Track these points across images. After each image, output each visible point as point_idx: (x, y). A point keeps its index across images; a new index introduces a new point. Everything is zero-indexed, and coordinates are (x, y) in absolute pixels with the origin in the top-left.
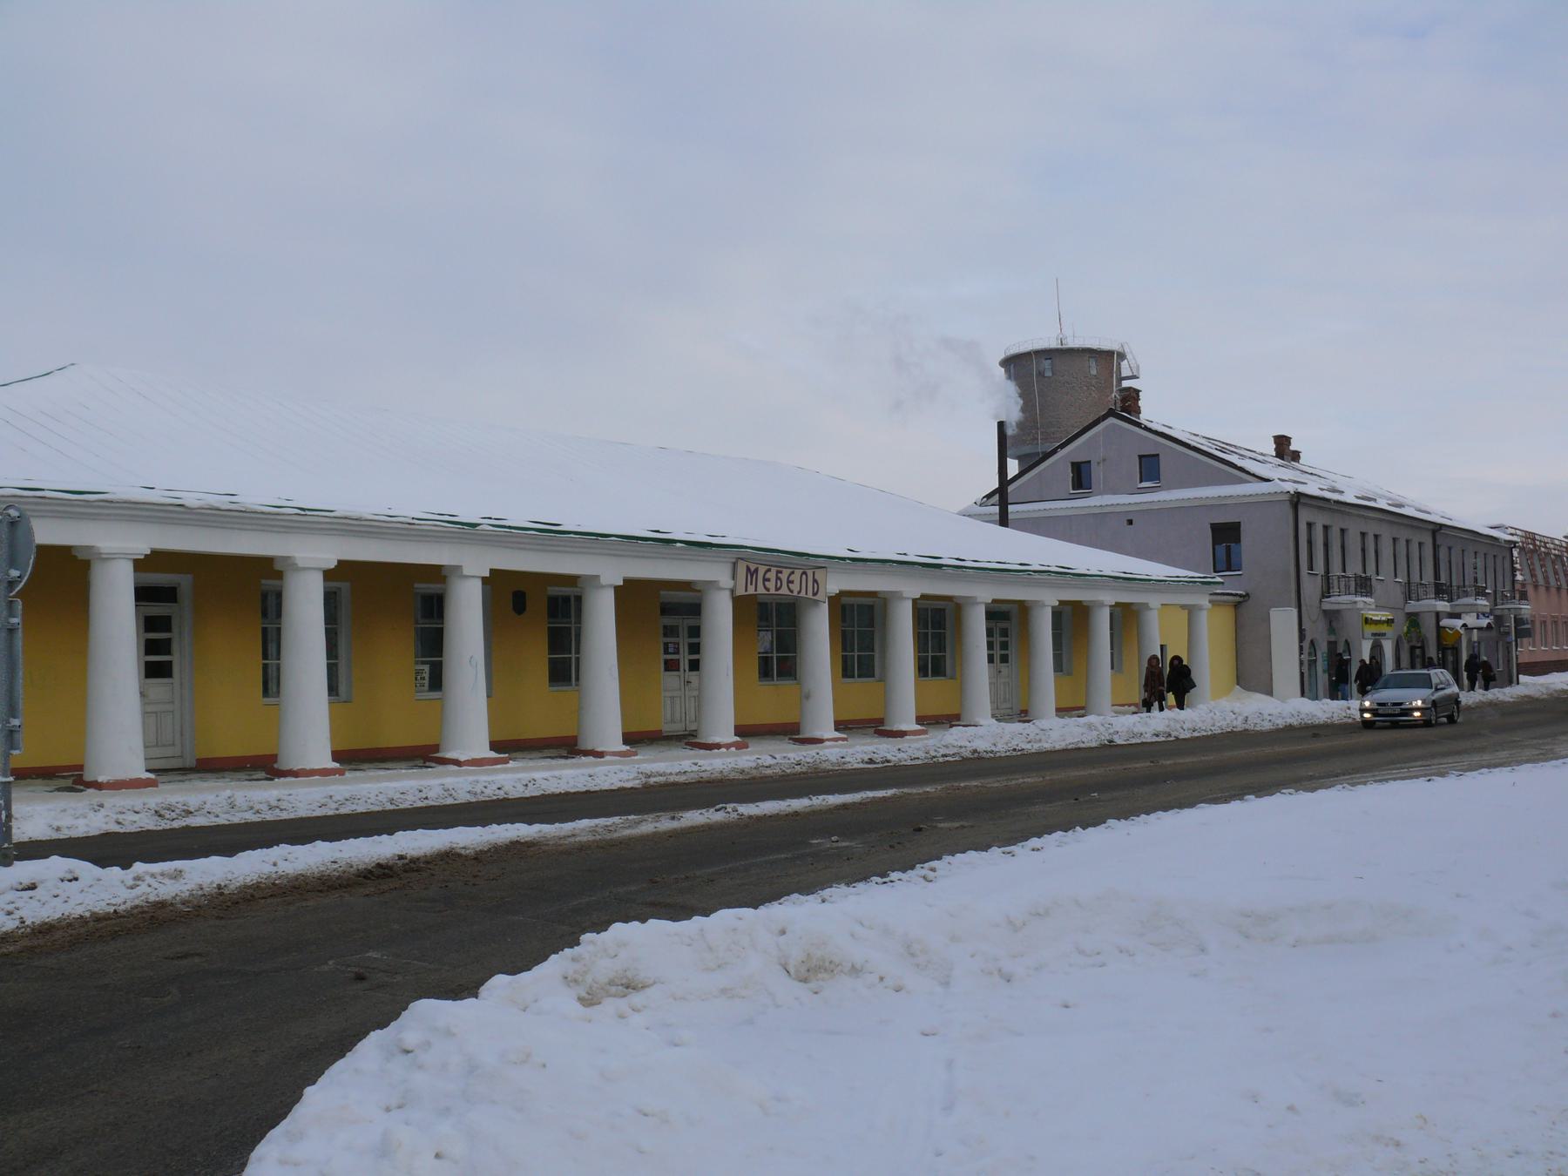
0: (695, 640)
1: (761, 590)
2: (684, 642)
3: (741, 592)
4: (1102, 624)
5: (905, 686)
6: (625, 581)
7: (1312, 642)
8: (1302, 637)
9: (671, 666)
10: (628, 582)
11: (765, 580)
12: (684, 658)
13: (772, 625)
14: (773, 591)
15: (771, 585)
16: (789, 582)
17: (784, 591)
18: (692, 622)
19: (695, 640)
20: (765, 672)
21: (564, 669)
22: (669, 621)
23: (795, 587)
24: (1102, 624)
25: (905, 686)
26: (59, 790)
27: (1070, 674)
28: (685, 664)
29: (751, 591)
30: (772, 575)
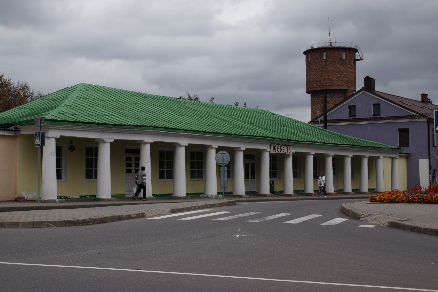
0: (137, 162)
1: (277, 152)
2: (133, 163)
3: (272, 152)
4: (181, 157)
5: (181, 183)
6: (246, 149)
7: (434, 170)
8: (430, 168)
9: (129, 171)
10: (61, 137)
11: (278, 149)
12: (133, 168)
13: (127, 156)
14: (279, 152)
15: (279, 150)
16: (284, 149)
17: (282, 152)
18: (136, 156)
19: (137, 162)
20: (162, 176)
21: (91, 172)
22: (129, 155)
23: (285, 151)
24: (181, 157)
25: (181, 183)
26: (430, 181)
27: (300, 178)
28: (133, 171)
29: (274, 152)
30: (279, 147)
